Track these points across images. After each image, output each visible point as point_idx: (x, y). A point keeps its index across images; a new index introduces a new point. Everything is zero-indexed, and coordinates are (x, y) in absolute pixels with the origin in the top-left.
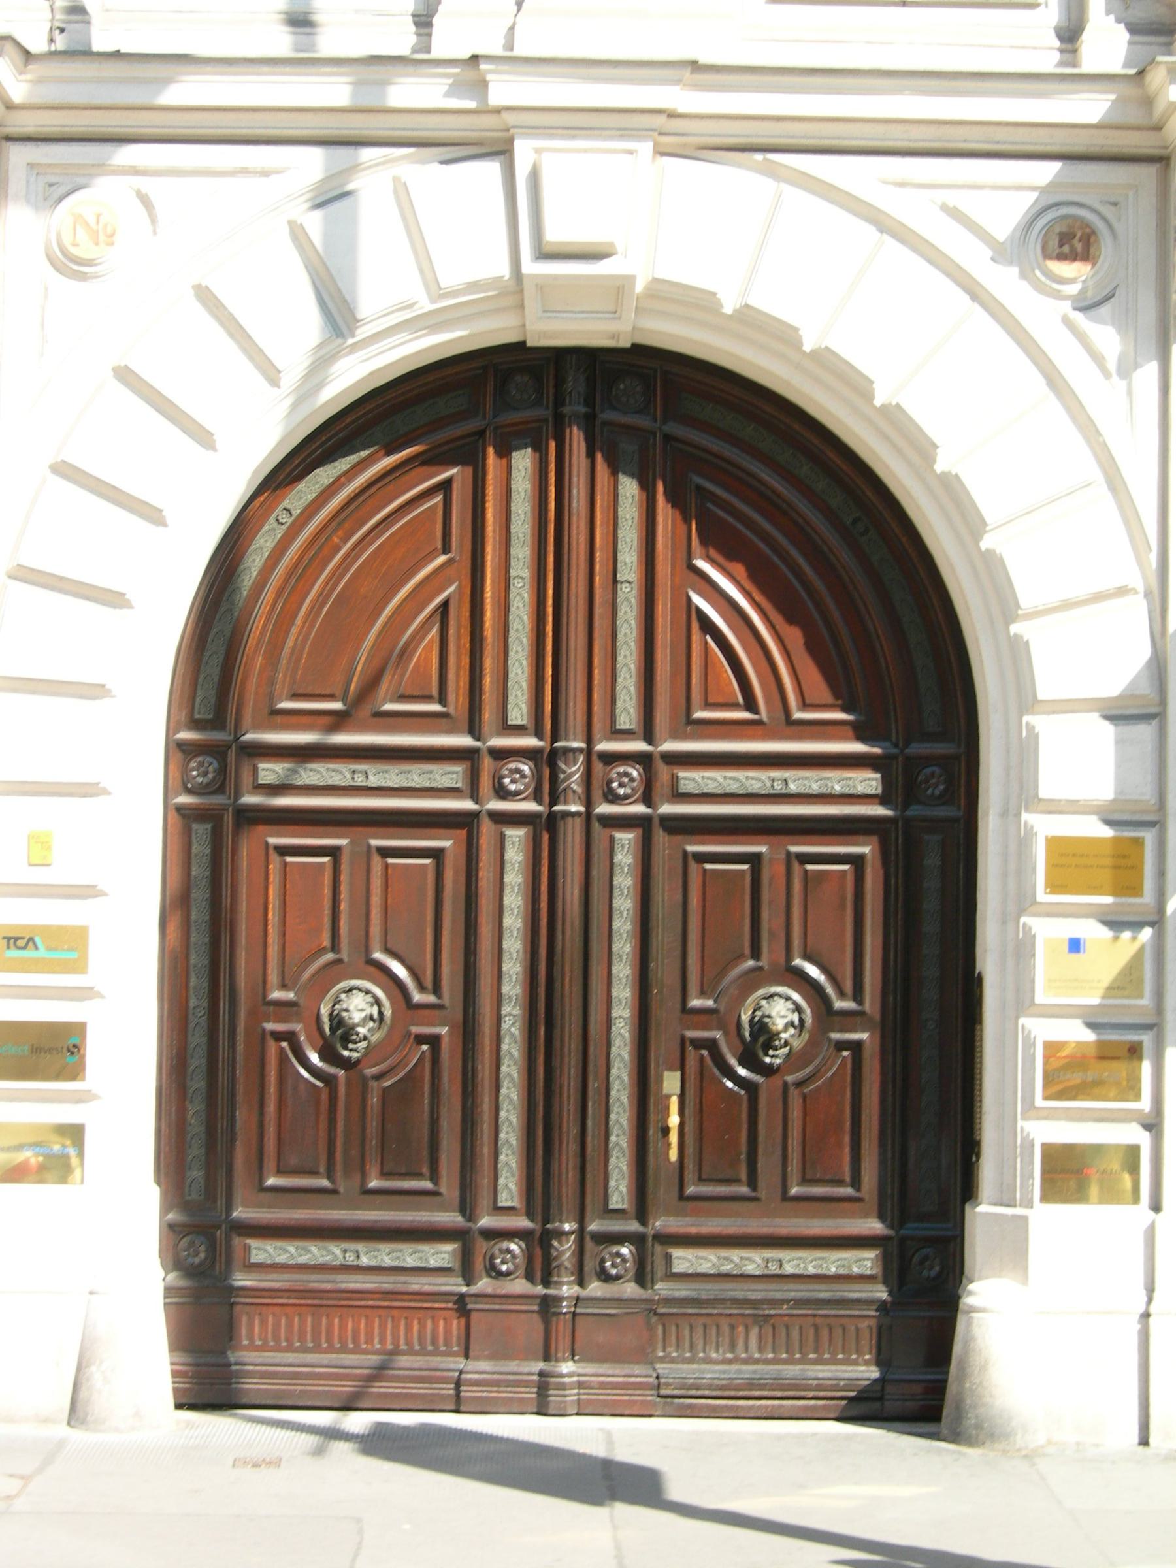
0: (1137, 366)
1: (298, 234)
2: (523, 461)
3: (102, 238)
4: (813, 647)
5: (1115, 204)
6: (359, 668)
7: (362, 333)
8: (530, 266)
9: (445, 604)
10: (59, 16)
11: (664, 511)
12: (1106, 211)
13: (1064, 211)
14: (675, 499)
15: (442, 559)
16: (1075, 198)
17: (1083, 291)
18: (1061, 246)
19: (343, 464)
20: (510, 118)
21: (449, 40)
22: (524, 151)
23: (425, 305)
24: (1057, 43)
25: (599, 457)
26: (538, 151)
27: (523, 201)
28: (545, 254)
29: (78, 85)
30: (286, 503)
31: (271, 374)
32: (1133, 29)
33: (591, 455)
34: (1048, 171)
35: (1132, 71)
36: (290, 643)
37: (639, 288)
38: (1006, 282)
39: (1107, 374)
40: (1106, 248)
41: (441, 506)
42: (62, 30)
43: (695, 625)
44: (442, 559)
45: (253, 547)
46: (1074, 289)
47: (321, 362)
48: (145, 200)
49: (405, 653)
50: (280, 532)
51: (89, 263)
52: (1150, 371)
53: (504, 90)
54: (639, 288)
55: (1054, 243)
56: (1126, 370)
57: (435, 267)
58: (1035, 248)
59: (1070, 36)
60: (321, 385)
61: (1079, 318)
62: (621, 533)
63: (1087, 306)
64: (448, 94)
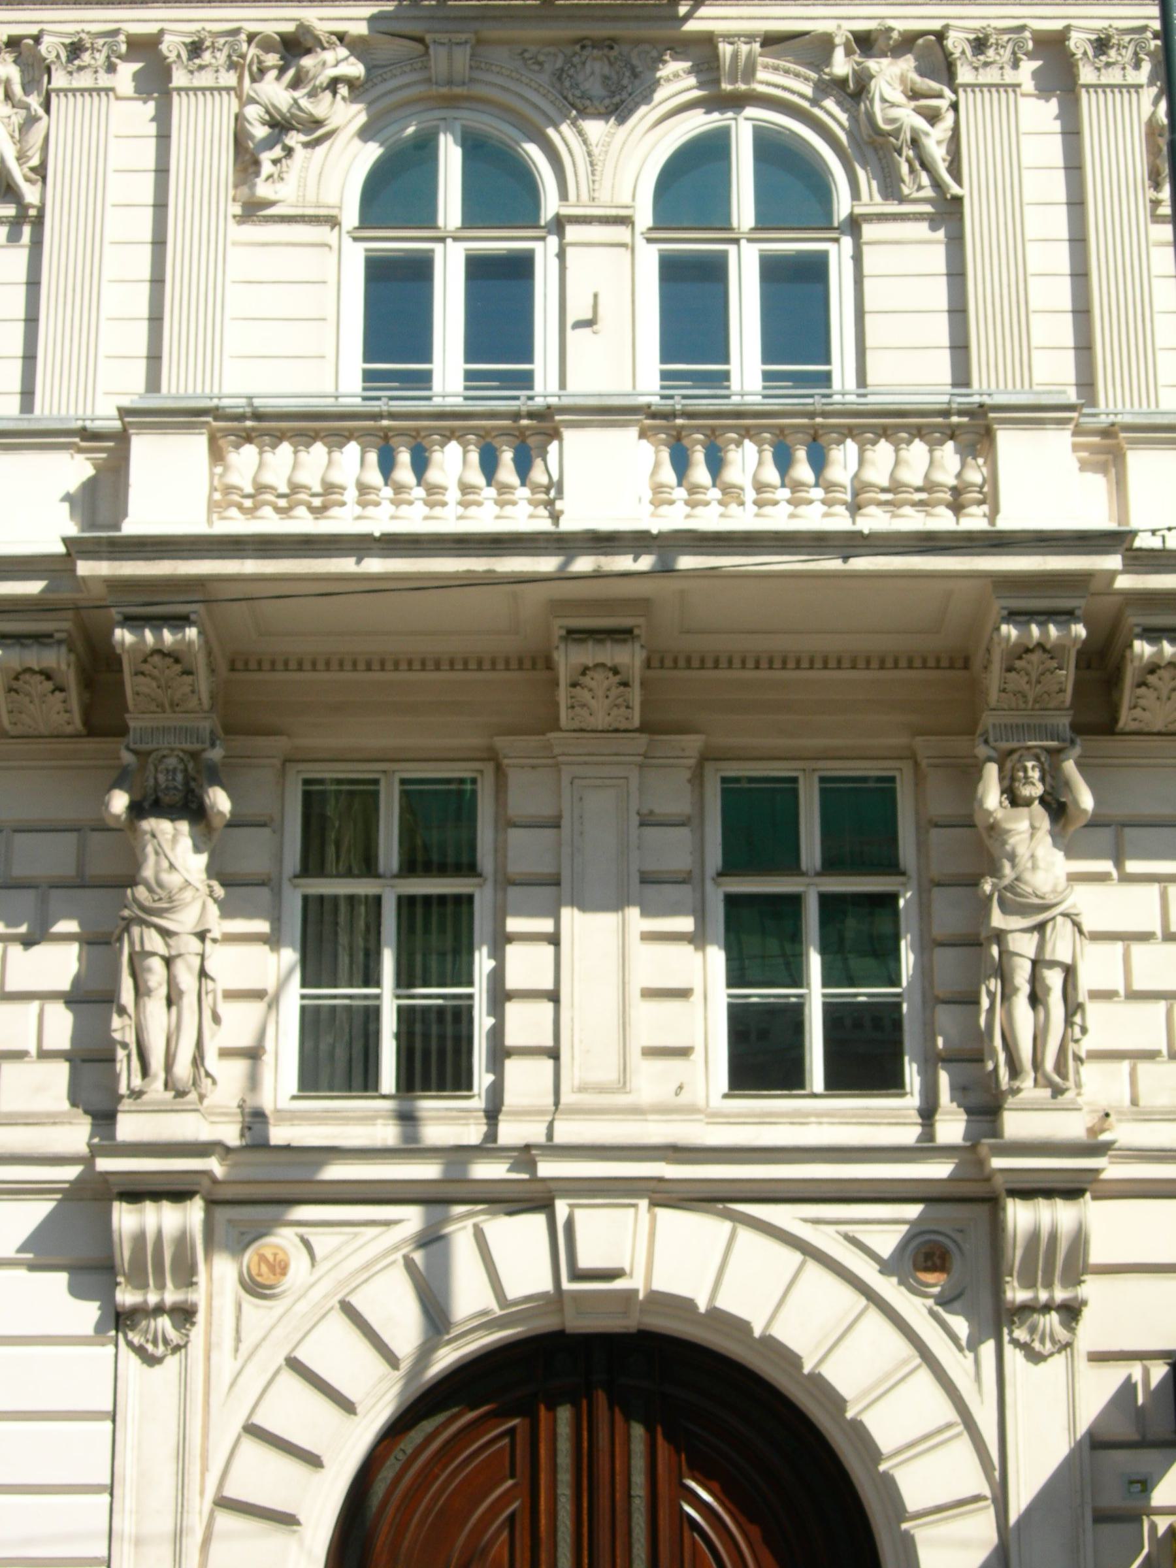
0: (981, 1342)
1: (409, 1264)
2: (564, 1414)
3: (278, 1270)
4: (768, 1541)
5: (961, 1231)
6: (454, 1560)
7: (454, 1332)
8: (566, 1285)
9: (512, 1517)
10: (247, 1119)
11: (662, 1446)
12: (958, 1237)
13: (927, 1237)
14: (668, 1437)
15: (510, 1483)
16: (935, 1228)
17: (941, 1292)
18: (926, 1261)
19: (441, 1418)
20: (552, 1185)
21: (510, 1133)
22: (562, 1208)
23: (498, 1312)
24: (919, 1121)
25: (617, 1410)
26: (571, 1206)
27: (562, 1242)
28: (578, 1275)
29: (258, 1168)
30: (402, 1446)
31: (392, 1360)
32: (969, 1111)
33: (611, 1408)
34: (913, 1211)
35: (968, 1144)
36: (406, 1543)
37: (641, 1296)
38: (889, 1288)
39: (960, 1349)
40: (956, 1263)
41: (508, 1449)
42: (250, 1128)
43: (686, 1526)
44: (510, 1483)
45: (380, 1477)
46: (936, 1290)
47: (425, 1353)
48: (307, 1244)
49: (485, 1551)
50: (398, 1466)
51: (270, 1287)
52: (988, 1349)
53: (547, 1169)
54: (641, 1296)
55: (921, 1259)
56: (973, 1345)
57: (507, 1268)
58: (908, 1264)
59: (928, 1113)
60: (426, 1367)
61: (939, 1309)
62: (633, 1462)
63: (945, 1301)
64: (509, 1170)
